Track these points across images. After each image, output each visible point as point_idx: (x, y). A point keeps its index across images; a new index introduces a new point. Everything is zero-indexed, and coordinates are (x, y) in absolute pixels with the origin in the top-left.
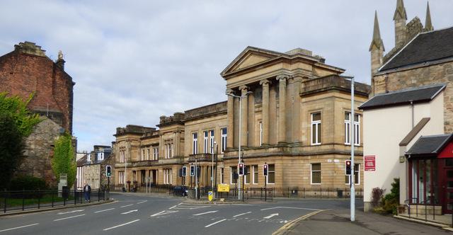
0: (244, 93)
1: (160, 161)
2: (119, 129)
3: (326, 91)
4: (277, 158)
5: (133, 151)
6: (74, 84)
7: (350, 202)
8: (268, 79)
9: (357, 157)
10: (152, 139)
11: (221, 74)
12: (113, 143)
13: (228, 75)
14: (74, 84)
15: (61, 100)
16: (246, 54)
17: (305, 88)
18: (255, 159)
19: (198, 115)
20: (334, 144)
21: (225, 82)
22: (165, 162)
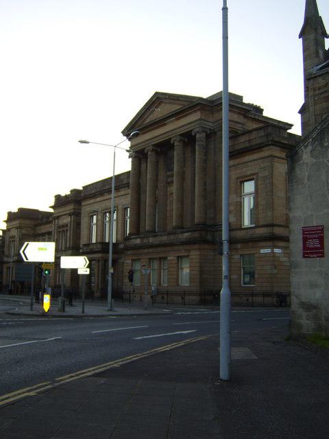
2: (58, 198)
7: (109, 248)
8: (180, 135)
11: (123, 132)
18: (163, 249)
20: (272, 225)
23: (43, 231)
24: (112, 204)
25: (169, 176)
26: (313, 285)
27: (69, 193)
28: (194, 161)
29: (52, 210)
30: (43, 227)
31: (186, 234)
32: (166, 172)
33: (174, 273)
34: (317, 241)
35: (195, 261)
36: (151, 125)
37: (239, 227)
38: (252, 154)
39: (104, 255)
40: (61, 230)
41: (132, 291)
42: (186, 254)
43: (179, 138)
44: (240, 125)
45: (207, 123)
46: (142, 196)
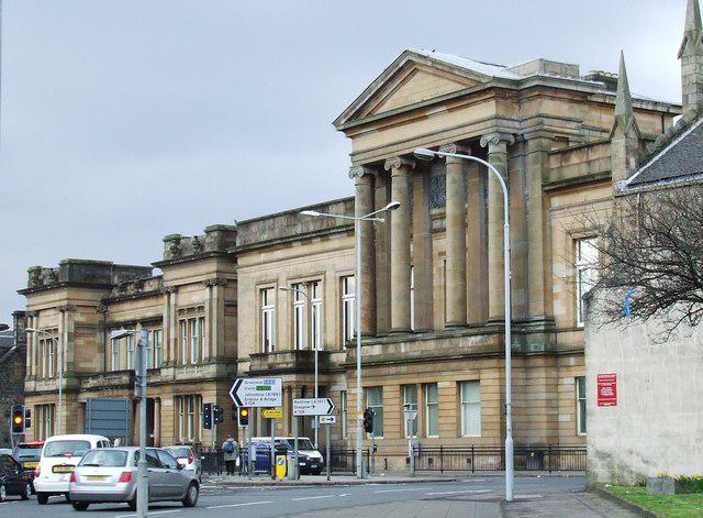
0: (398, 182)
1: (164, 372)
2: (36, 273)
5: (81, 342)
9: (369, 371)
10: (142, 304)
11: (336, 123)
12: (19, 315)
13: (356, 121)
18: (429, 367)
21: (346, 145)
22: (183, 375)
23: (129, 317)
25: (433, 218)
26: (607, 434)
28: (486, 191)
30: (127, 306)
31: (473, 338)
33: (453, 413)
34: (610, 389)
35: (491, 389)
37: (572, 325)
38: (594, 188)
39: (301, 378)
40: (186, 317)
41: (371, 450)
42: (474, 377)
44: (574, 125)
45: (510, 123)
46: (379, 255)
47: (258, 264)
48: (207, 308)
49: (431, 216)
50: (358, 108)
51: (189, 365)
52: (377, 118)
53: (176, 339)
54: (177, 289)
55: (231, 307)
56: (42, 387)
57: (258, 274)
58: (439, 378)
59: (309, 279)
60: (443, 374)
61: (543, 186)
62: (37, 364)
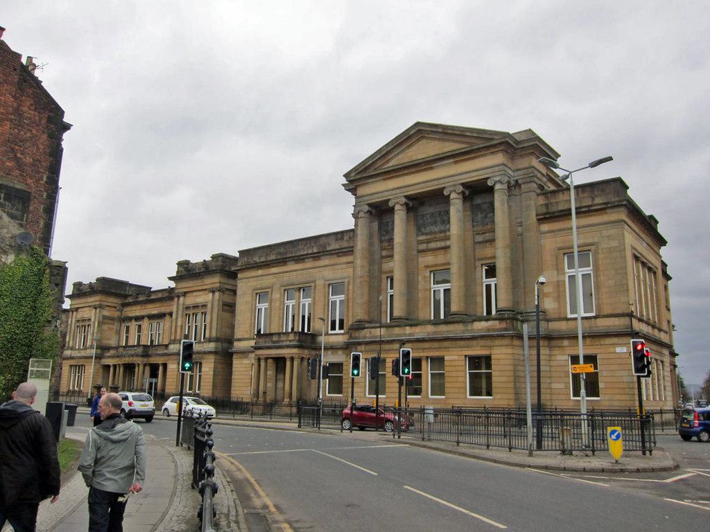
2: (184, 265)
3: (603, 209)
4: (497, 342)
5: (105, 327)
6: (67, 127)
8: (463, 185)
9: (588, 341)
10: (150, 306)
13: (356, 180)
14: (67, 127)
15: (29, 160)
16: (410, 137)
17: (547, 205)
18: (436, 345)
19: (273, 257)
23: (138, 314)
24: (576, 240)
27: (94, 281)
29: (172, 284)
32: (418, 235)
36: (394, 171)
40: (81, 324)
43: (404, 200)
47: (257, 277)
48: (209, 306)
49: (418, 241)
50: (367, 165)
51: (79, 349)
52: (382, 171)
53: (182, 326)
54: (185, 294)
55: (230, 307)
56: (76, 354)
57: (255, 283)
58: (448, 353)
59: (301, 286)
60: (451, 350)
61: (537, 215)
62: (73, 340)
